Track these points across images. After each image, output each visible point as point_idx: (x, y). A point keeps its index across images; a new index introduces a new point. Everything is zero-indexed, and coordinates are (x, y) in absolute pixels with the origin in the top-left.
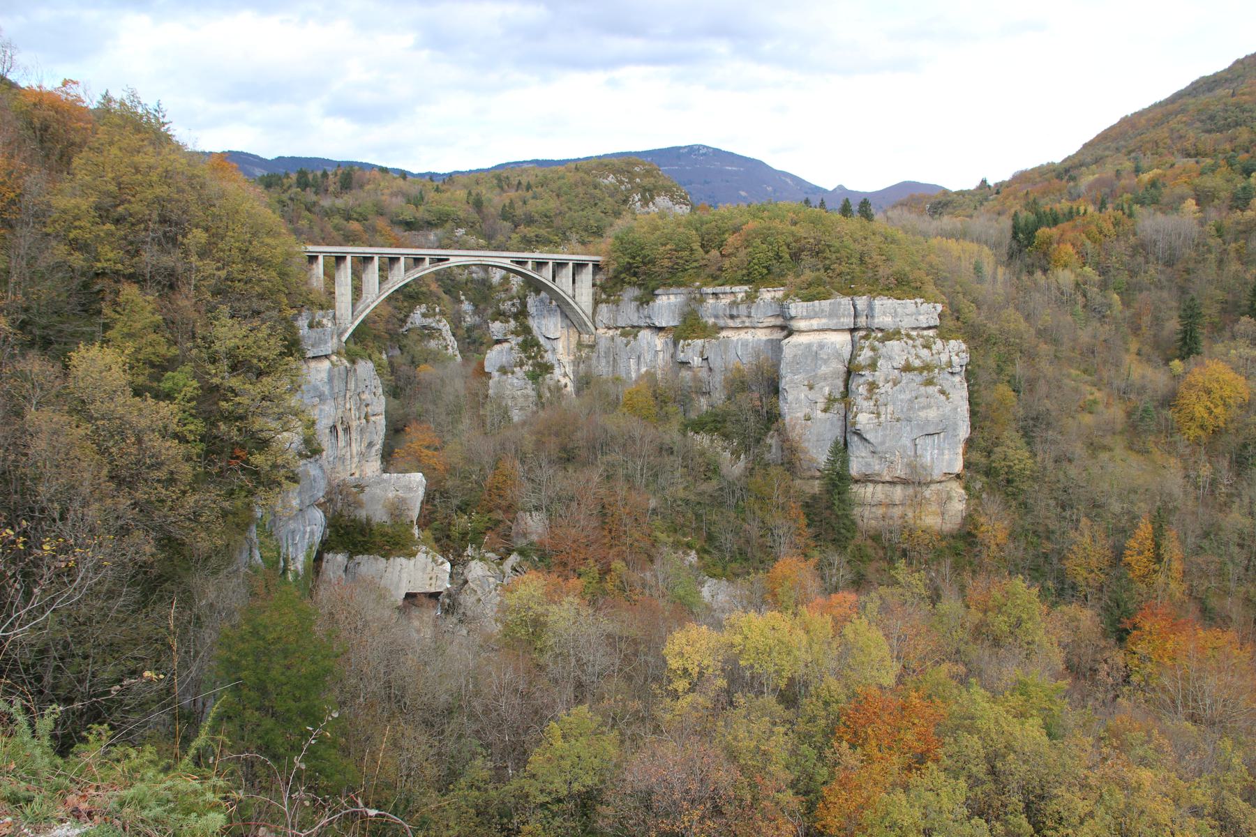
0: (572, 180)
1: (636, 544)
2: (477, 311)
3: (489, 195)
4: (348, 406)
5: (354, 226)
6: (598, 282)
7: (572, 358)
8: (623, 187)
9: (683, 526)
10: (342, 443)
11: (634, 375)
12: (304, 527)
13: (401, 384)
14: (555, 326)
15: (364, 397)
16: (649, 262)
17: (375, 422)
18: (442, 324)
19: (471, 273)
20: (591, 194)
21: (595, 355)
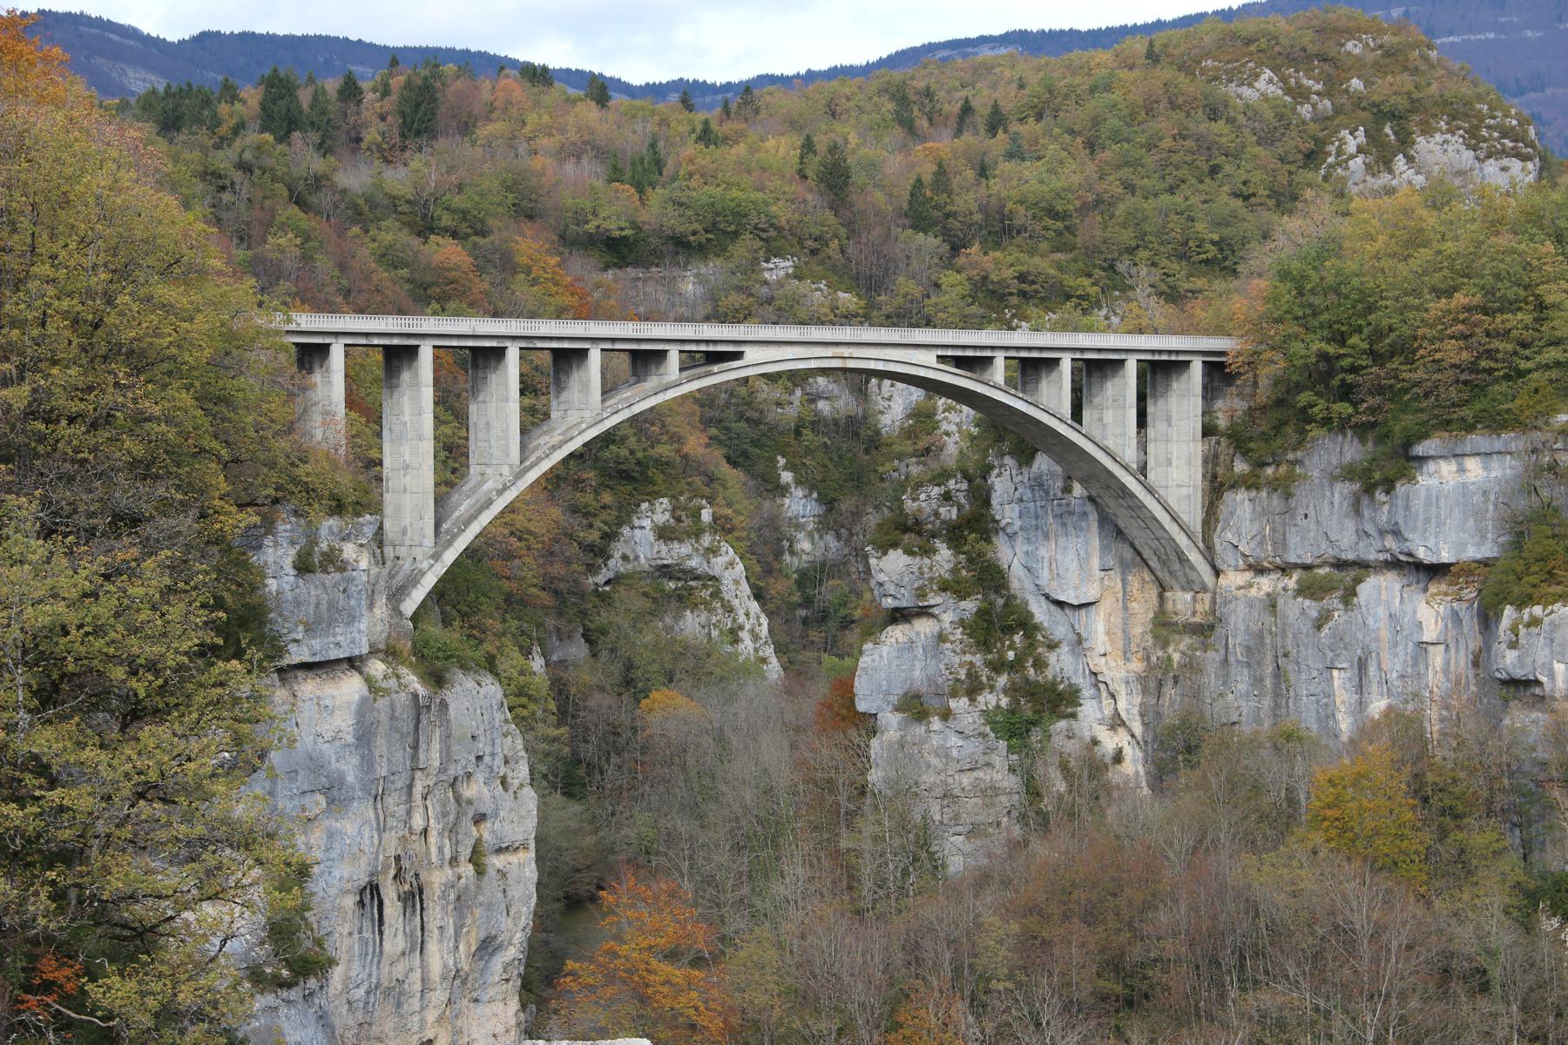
2: (830, 520)
3: (868, 152)
4: (418, 822)
5: (446, 252)
6: (1222, 422)
7: (1137, 666)
8: (1305, 110)
10: (395, 942)
11: (1345, 724)
13: (589, 751)
14: (1083, 562)
15: (468, 791)
17: (502, 874)
18: (719, 562)
19: (813, 399)
21: (1213, 657)
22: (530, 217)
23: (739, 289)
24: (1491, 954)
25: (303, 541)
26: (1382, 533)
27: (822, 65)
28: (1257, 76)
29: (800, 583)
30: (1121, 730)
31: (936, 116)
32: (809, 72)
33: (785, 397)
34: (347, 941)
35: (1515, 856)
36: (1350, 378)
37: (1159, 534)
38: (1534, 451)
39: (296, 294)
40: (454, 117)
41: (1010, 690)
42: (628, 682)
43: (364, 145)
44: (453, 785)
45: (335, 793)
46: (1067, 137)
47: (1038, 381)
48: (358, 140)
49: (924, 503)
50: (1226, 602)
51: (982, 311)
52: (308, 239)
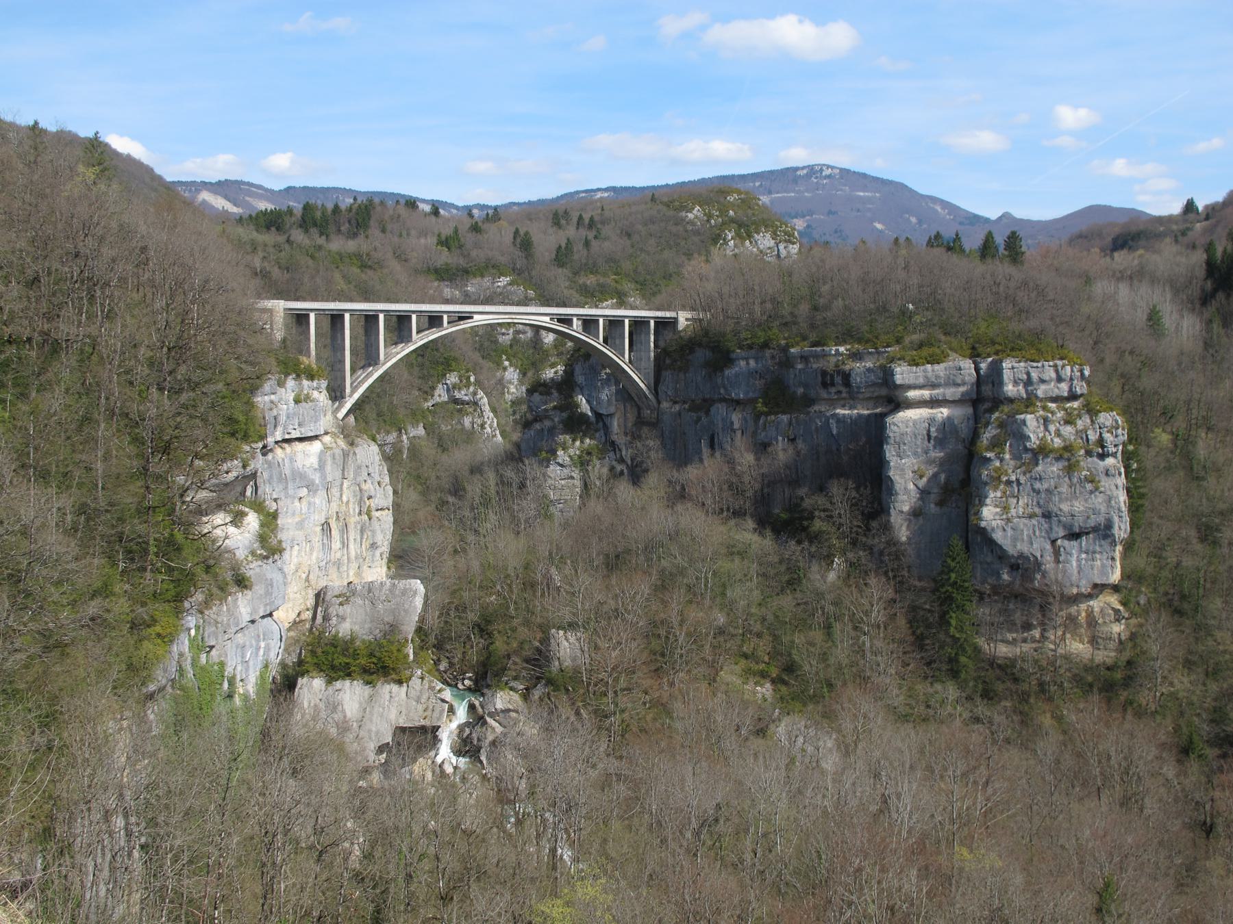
4: (345, 499)
10: (336, 545)
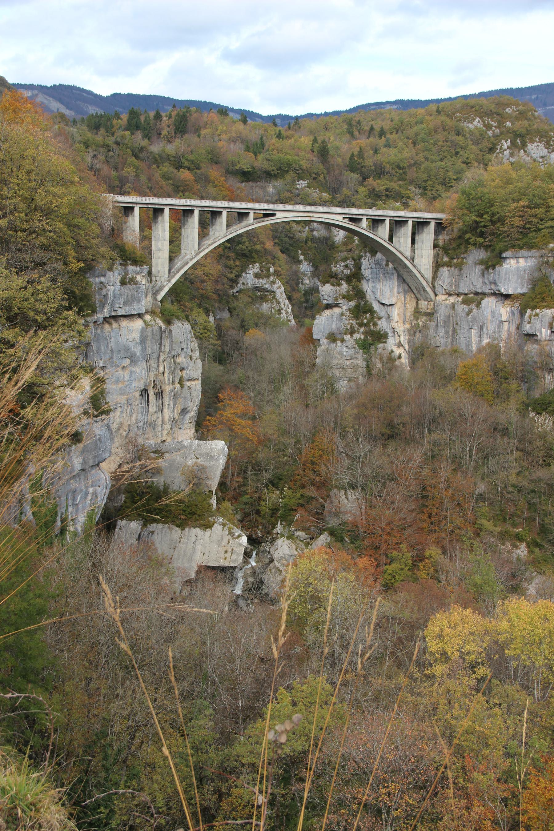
0: (431, 126)
1: (457, 531)
2: (316, 273)
3: (337, 143)
4: (161, 369)
5: (185, 175)
6: (441, 243)
7: (408, 326)
8: (490, 133)
9: (513, 515)
10: (153, 408)
11: (474, 347)
12: (87, 487)
13: (228, 349)
14: (391, 290)
15: (178, 360)
16: (499, 220)
17: (190, 388)
18: (275, 286)
19: (312, 230)
20: (452, 142)
21: (433, 324)
22: (216, 163)
23: (288, 191)
24: (510, 423)
25: (123, 274)
26: (491, 283)
27: (330, 110)
28: (474, 120)
29: (304, 295)
30: (401, 348)
31: (361, 131)
32: (325, 112)
33: (302, 229)
34: (137, 407)
35: (523, 392)
36: (483, 229)
37: (417, 281)
38: (542, 256)
39: (133, 188)
40: (193, 126)
41: (365, 333)
42: (242, 326)
43: (162, 136)
44: (173, 358)
45: (133, 358)
46: (406, 140)
47: (378, 227)
48: (160, 134)
49: (338, 268)
50: (438, 305)
51: (372, 201)
52: (138, 169)
